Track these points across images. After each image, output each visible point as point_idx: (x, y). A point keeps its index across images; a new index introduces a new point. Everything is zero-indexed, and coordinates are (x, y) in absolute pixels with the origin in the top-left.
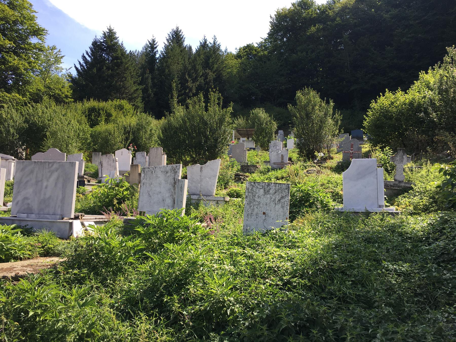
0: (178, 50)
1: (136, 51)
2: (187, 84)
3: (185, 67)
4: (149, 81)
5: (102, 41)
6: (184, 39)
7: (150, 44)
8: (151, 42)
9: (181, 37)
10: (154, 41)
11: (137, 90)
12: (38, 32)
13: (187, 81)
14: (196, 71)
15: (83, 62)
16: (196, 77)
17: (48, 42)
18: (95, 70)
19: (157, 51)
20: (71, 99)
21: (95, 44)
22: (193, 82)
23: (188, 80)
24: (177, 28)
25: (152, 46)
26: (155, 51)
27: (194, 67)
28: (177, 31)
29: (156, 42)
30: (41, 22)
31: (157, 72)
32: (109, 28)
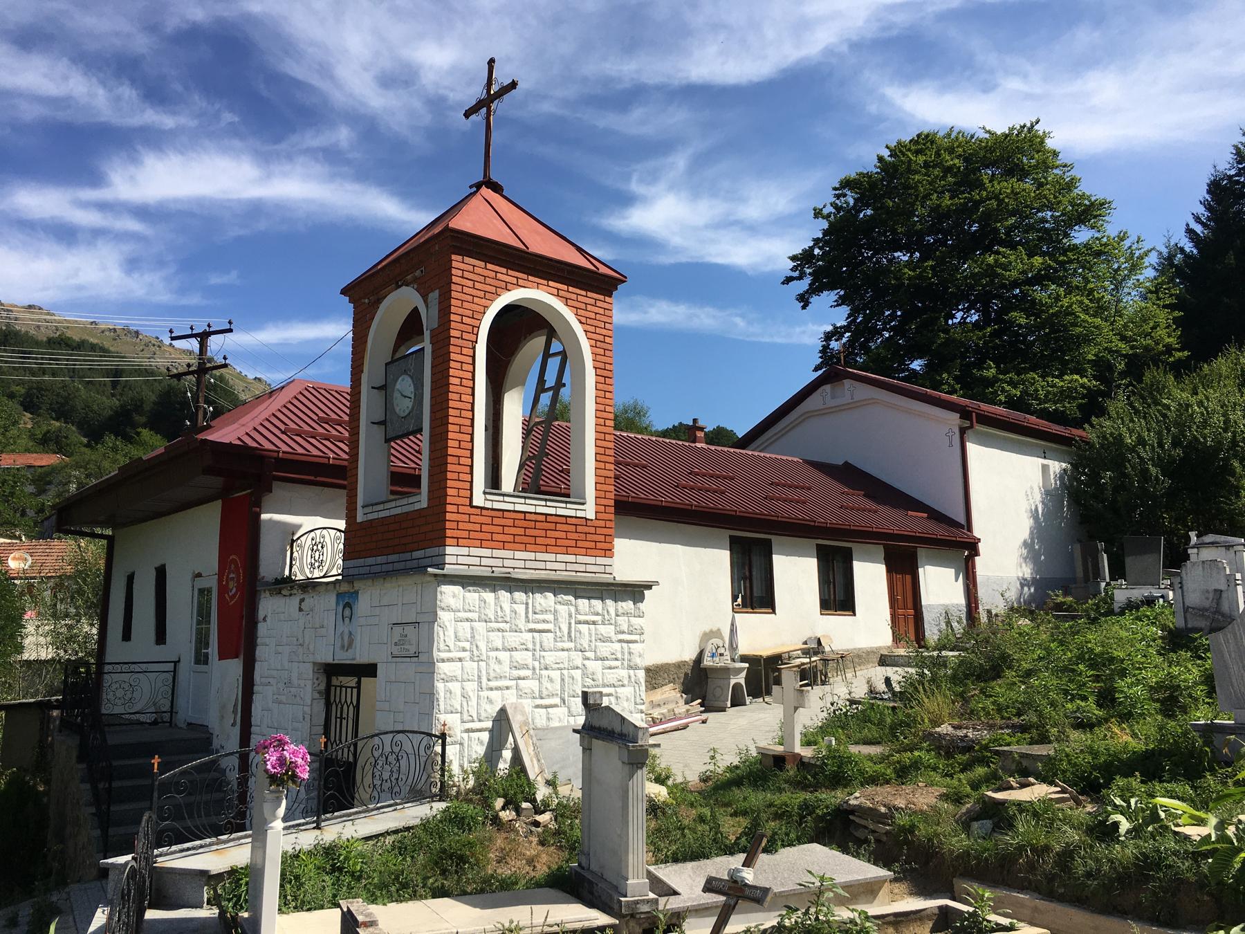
5: (1233, 172)
12: (1089, 212)
15: (1191, 245)
17: (1111, 228)
21: (1215, 187)
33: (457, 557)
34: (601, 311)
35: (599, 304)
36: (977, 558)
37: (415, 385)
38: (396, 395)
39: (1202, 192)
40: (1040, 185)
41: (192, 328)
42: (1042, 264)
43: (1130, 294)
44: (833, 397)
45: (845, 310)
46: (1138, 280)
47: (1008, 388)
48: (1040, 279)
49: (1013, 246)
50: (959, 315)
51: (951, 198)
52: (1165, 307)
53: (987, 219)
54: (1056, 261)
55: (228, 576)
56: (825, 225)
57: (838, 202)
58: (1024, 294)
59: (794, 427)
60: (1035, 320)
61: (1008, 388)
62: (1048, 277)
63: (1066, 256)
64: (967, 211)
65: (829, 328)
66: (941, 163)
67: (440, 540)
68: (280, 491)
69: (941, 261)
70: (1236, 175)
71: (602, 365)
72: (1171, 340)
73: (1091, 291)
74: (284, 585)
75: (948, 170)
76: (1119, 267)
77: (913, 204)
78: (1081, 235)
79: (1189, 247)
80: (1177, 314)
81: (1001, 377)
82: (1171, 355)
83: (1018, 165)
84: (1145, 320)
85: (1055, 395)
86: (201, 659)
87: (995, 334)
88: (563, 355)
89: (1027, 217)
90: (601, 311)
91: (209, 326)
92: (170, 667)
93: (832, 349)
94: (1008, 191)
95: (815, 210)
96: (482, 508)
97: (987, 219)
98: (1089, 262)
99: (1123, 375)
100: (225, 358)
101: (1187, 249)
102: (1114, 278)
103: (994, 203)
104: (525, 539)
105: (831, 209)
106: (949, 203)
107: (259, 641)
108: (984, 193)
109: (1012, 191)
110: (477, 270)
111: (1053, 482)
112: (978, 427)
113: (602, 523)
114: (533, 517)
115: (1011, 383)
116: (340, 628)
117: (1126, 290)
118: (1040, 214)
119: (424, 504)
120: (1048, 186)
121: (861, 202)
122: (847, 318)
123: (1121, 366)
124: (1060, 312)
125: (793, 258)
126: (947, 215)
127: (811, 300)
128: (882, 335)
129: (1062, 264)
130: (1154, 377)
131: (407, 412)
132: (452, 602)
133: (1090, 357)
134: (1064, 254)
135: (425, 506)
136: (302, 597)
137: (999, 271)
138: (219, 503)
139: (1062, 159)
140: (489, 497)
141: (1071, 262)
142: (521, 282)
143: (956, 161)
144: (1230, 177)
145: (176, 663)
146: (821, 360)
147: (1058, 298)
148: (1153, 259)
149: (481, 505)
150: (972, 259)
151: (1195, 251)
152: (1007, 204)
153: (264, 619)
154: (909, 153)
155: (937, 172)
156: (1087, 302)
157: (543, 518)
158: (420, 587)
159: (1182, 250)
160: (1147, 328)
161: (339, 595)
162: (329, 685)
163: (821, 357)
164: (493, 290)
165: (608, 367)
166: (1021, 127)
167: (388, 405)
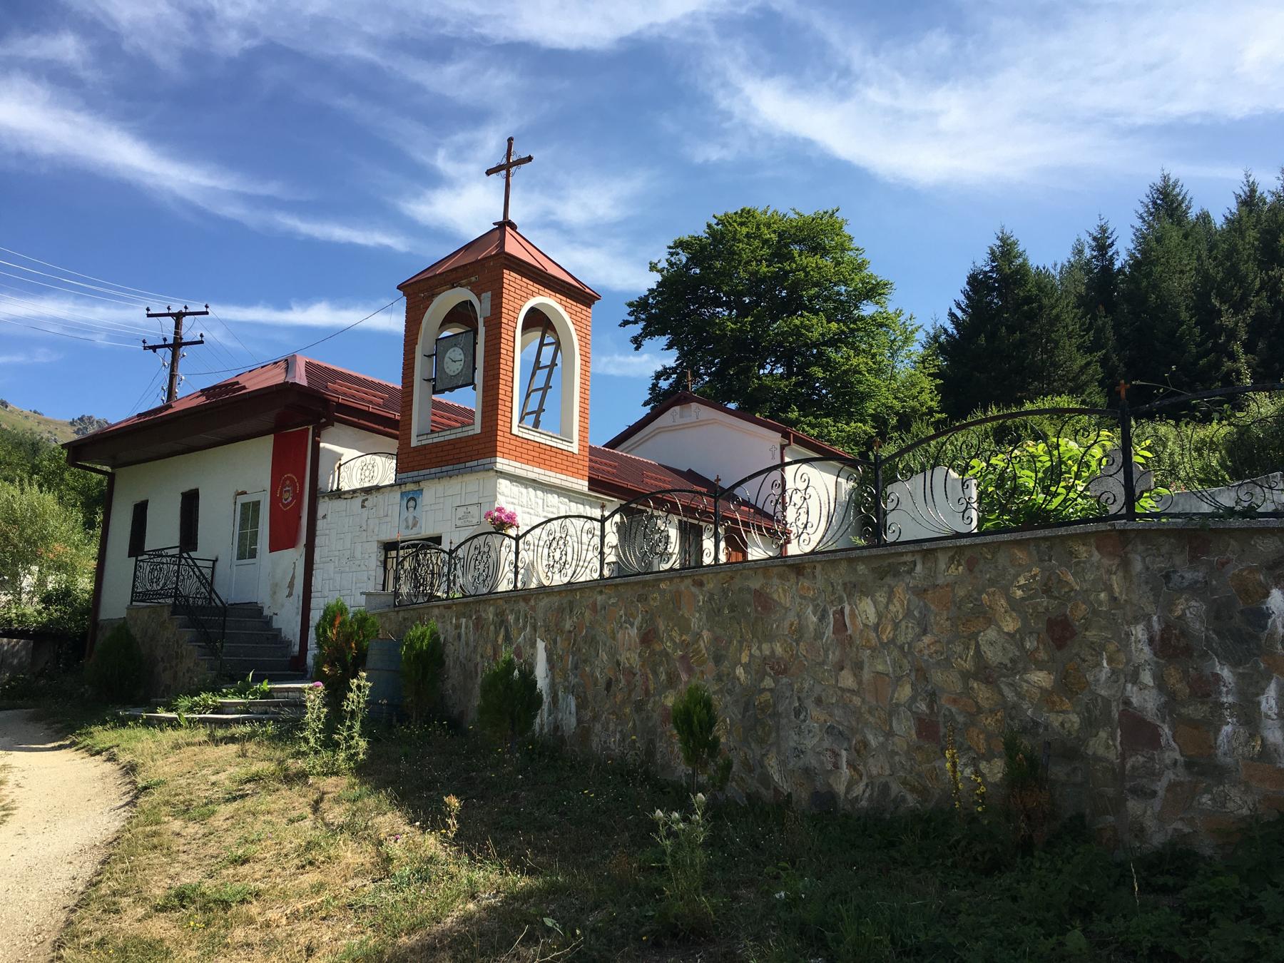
0: (1175, 236)
1: (1056, 265)
2: (1217, 322)
3: (1206, 277)
4: (1108, 335)
5: (988, 269)
6: (1190, 202)
7: (1095, 239)
8: (1095, 234)
9: (1180, 198)
10: (1103, 230)
11: (1088, 364)
12: (873, 291)
13: (1219, 314)
14: (1241, 280)
16: (1244, 297)
18: (982, 340)
19: (1117, 253)
20: (940, 415)
21: (973, 280)
22: (1235, 314)
23: (1220, 310)
24: (1166, 179)
25: (1102, 244)
26: (1110, 254)
27: (1233, 273)
28: (1166, 186)
29: (1110, 231)
30: (877, 270)
31: (1125, 308)
32: (1000, 235)
33: (502, 463)
34: (584, 317)
35: (583, 312)
36: (788, 545)
37: (465, 354)
38: (446, 359)
39: (963, 284)
40: (838, 264)
41: (169, 308)
42: (838, 329)
43: (902, 361)
44: (682, 417)
45: (675, 353)
46: (910, 351)
47: (807, 429)
48: (834, 342)
49: (816, 313)
50: (769, 367)
51: (767, 266)
52: (929, 375)
53: (795, 288)
54: (848, 328)
55: (282, 489)
56: (658, 277)
57: (672, 259)
58: (821, 354)
59: (647, 440)
60: (830, 375)
61: (807, 429)
62: (840, 340)
63: (856, 324)
64: (780, 277)
65: (660, 368)
66: (760, 236)
67: (493, 453)
68: (337, 430)
69: (758, 318)
70: (990, 271)
71: (584, 353)
72: (933, 403)
73: (874, 356)
74: (338, 494)
75: (765, 242)
76: (895, 339)
77: (736, 268)
78: (868, 309)
79: (951, 328)
80: (939, 381)
81: (802, 419)
82: (932, 416)
83: (820, 244)
84: (913, 385)
85: (843, 438)
86: (247, 551)
87: (798, 384)
88: (558, 345)
89: (826, 289)
90: (584, 317)
91: (186, 308)
92: (210, 564)
93: (660, 388)
94: (814, 265)
95: (651, 264)
96: (517, 436)
97: (795, 288)
98: (873, 332)
99: (895, 428)
100: (202, 336)
101: (950, 330)
102: (891, 347)
103: (802, 274)
104: (540, 460)
105: (666, 265)
106: (766, 270)
107: (318, 533)
108: (794, 265)
109: (817, 266)
110: (517, 281)
111: (844, 497)
112: (794, 446)
113: (581, 457)
114: (544, 447)
115: (810, 425)
116: (403, 517)
117: (900, 358)
118: (835, 288)
119: (478, 430)
120: (844, 265)
121: (693, 260)
122: (676, 361)
123: (894, 421)
124: (849, 370)
125: (630, 305)
126: (763, 280)
127: (643, 343)
128: (703, 380)
129: (852, 331)
130: (919, 428)
131: (457, 372)
132: (506, 491)
133: (871, 411)
134: (854, 323)
135: (479, 431)
136: (364, 498)
137: (804, 331)
138: (270, 439)
139: (855, 244)
140: (521, 429)
141: (859, 330)
142: (541, 292)
143: (773, 235)
144: (986, 273)
145: (215, 561)
146: (650, 396)
147: (848, 359)
148: (921, 336)
149: (516, 434)
150: (782, 320)
151: (955, 332)
152: (812, 277)
153: (324, 517)
154: (735, 224)
155: (757, 243)
156: (871, 363)
157: (549, 448)
158: (481, 481)
159: (945, 330)
160: (915, 391)
161: (403, 494)
162: (386, 558)
163: (650, 394)
164: (525, 295)
165: (588, 355)
166: (824, 213)
167: (439, 367)
